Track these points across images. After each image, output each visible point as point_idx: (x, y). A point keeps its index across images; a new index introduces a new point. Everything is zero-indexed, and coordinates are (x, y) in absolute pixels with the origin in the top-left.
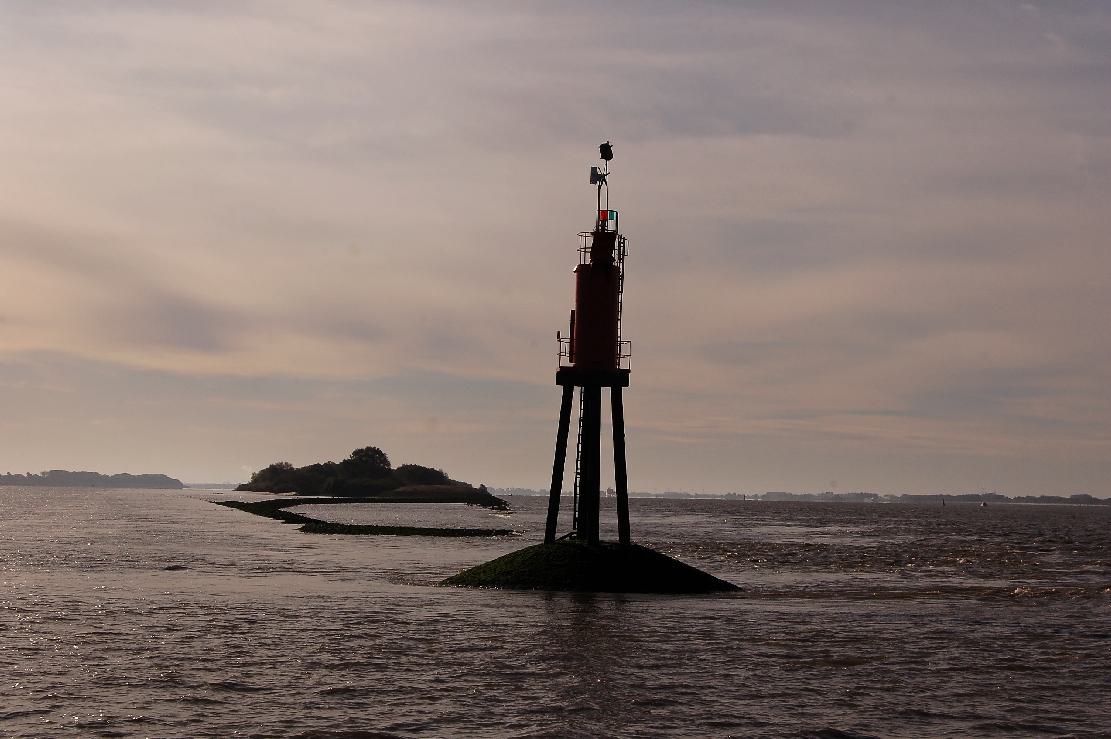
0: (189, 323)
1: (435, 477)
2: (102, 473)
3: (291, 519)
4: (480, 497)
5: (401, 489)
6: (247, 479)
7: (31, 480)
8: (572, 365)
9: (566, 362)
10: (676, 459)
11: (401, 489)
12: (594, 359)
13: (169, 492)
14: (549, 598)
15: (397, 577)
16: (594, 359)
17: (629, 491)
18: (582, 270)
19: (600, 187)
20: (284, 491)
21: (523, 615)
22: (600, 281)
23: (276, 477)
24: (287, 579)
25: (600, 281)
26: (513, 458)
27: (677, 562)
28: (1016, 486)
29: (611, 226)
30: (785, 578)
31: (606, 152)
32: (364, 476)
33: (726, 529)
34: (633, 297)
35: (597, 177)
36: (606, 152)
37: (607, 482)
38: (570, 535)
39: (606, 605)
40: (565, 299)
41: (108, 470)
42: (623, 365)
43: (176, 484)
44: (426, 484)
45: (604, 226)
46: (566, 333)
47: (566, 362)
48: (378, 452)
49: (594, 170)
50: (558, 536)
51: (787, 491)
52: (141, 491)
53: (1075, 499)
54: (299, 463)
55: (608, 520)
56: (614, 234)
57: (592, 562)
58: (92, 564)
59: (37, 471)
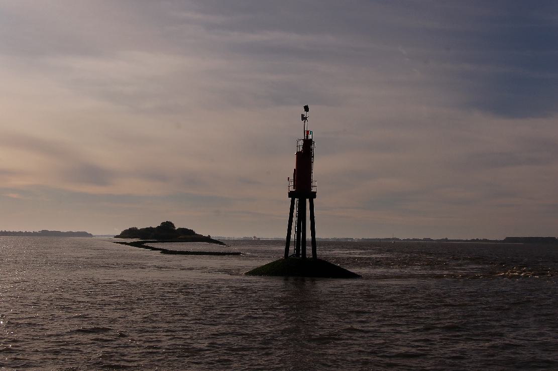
0: (94, 174)
1: (191, 232)
2: (62, 231)
3: (147, 247)
4: (208, 240)
5: (180, 237)
6: (119, 234)
7: (35, 234)
8: (294, 190)
9: (292, 189)
10: (332, 224)
11: (180, 237)
12: (302, 189)
13: (88, 238)
14: (286, 280)
15: (228, 271)
16: (302, 189)
17: (307, 238)
18: (298, 154)
19: (305, 122)
20: (140, 237)
21: (276, 283)
22: (305, 158)
23: (130, 233)
24: (189, 272)
25: (305, 158)
26: (272, 225)
27: (338, 267)
28: (403, 235)
29: (310, 137)
30: (380, 271)
31: (306, 109)
32: (166, 233)
33: (356, 253)
34: (319, 167)
35: (304, 118)
36: (306, 109)
37: (309, 236)
38: (293, 255)
39: (308, 283)
40: (291, 165)
41: (64, 229)
42: (313, 190)
43: (90, 235)
44: (188, 235)
45: (307, 137)
46: (292, 178)
47: (292, 189)
48: (171, 223)
49: (303, 115)
50: (289, 255)
51: (319, 237)
52: (81, 238)
53: (425, 240)
54: (140, 226)
55: (309, 251)
56: (311, 139)
57: (301, 264)
58: (107, 266)
59: (37, 231)
